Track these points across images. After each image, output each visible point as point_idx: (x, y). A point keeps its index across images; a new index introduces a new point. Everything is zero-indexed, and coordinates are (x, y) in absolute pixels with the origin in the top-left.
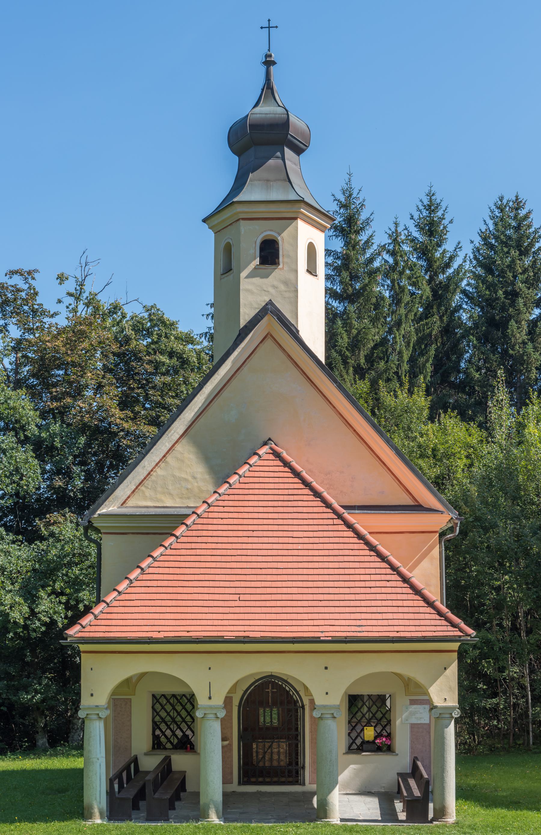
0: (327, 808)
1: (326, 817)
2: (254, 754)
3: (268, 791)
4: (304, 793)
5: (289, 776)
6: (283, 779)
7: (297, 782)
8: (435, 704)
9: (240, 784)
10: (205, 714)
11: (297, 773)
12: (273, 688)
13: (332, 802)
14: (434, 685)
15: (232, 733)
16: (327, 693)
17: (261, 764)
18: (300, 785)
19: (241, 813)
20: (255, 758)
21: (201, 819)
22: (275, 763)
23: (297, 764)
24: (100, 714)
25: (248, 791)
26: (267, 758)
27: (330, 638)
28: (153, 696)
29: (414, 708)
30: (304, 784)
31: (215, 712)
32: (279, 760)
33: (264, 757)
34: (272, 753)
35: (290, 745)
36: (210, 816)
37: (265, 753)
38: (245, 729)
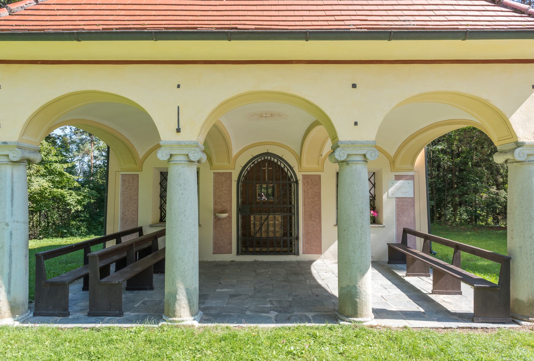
0: (358, 300)
1: (355, 315)
2: (252, 226)
3: (265, 260)
4: (298, 263)
5: (284, 247)
6: (278, 249)
7: (291, 251)
8: (521, 140)
9: (238, 253)
10: (171, 155)
11: (291, 243)
12: (269, 166)
13: (365, 292)
14: (518, 111)
15: (231, 206)
16: (356, 124)
17: (258, 235)
18: (295, 254)
19: (232, 296)
20: (252, 229)
21: (164, 317)
22: (271, 235)
23: (291, 234)
24: (11, 156)
25: (246, 260)
26: (263, 230)
27: (366, 30)
28: (161, 173)
29: (399, 183)
30: (298, 254)
31: (185, 152)
32: (274, 232)
33: (260, 228)
34: (268, 225)
35: (284, 218)
36: (177, 314)
37: (262, 224)
38: (243, 203)
